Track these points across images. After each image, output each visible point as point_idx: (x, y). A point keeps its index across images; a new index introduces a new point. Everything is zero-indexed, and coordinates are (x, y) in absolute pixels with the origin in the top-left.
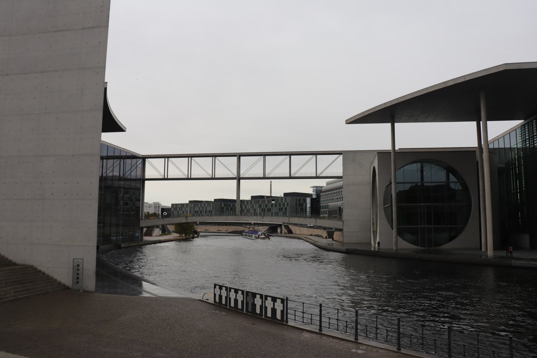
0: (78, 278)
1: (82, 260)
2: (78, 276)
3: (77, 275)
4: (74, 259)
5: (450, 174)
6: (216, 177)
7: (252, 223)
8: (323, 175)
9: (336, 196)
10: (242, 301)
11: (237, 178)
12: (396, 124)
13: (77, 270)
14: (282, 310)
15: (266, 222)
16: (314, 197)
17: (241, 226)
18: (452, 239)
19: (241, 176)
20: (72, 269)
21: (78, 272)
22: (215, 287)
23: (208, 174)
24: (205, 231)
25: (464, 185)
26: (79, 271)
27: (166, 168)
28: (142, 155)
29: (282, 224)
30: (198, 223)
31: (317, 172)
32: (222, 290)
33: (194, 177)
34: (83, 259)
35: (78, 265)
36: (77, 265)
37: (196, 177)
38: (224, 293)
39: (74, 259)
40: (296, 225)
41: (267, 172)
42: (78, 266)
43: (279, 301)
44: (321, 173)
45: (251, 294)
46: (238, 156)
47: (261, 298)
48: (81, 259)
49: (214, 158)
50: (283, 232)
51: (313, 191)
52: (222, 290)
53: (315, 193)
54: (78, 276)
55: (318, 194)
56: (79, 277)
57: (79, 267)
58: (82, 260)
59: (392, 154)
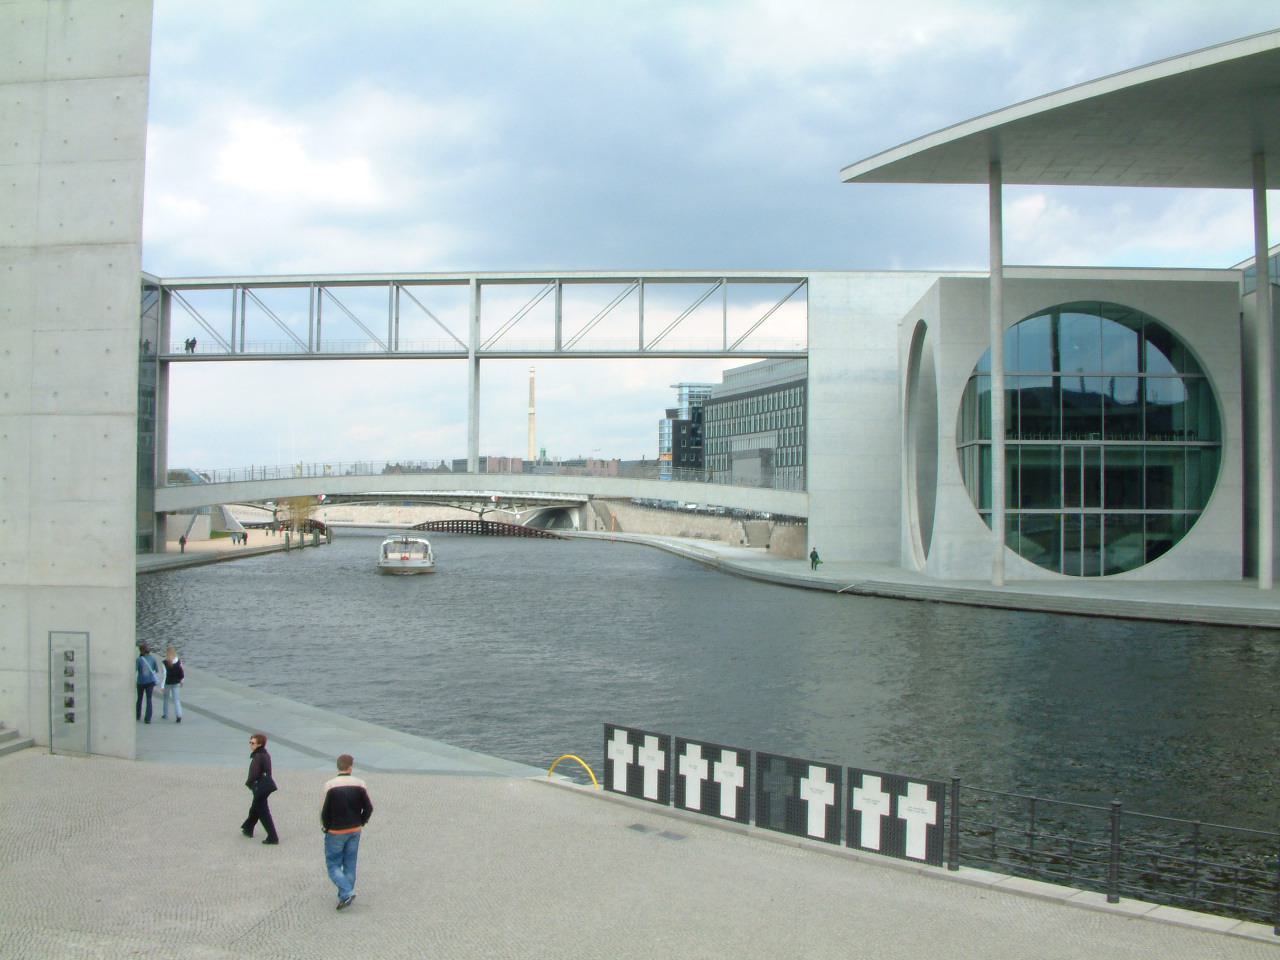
0: (70, 703)
1: (84, 636)
2: (70, 694)
3: (67, 691)
4: (53, 635)
5: (1149, 343)
6: (323, 350)
7: (493, 499)
8: (662, 347)
9: (755, 415)
10: (738, 789)
11: (472, 356)
12: (1005, 188)
13: (66, 672)
14: (832, 803)
15: (536, 496)
16: (685, 417)
17: (448, 505)
18: (1155, 551)
19: (483, 349)
20: (47, 675)
21: (71, 680)
22: (609, 734)
23: (298, 341)
24: (377, 524)
25: (1200, 386)
26: (72, 675)
27: (239, 324)
28: (160, 279)
29: (586, 499)
30: (324, 497)
31: (728, 339)
32: (716, 764)
33: (330, 350)
34: (87, 634)
35: (69, 654)
36: (66, 654)
37: (260, 351)
38: (619, 751)
39: (50, 633)
40: (627, 501)
41: (566, 337)
42: (69, 656)
43: (651, 742)
44: (656, 341)
45: (784, 764)
46: (473, 282)
47: (661, 747)
48: (82, 633)
49: (240, 291)
50: (591, 525)
51: (680, 400)
52: (716, 764)
53: (686, 405)
54: (70, 694)
55: (698, 408)
56: (75, 700)
57: (72, 660)
58: (84, 636)
59: (995, 286)
